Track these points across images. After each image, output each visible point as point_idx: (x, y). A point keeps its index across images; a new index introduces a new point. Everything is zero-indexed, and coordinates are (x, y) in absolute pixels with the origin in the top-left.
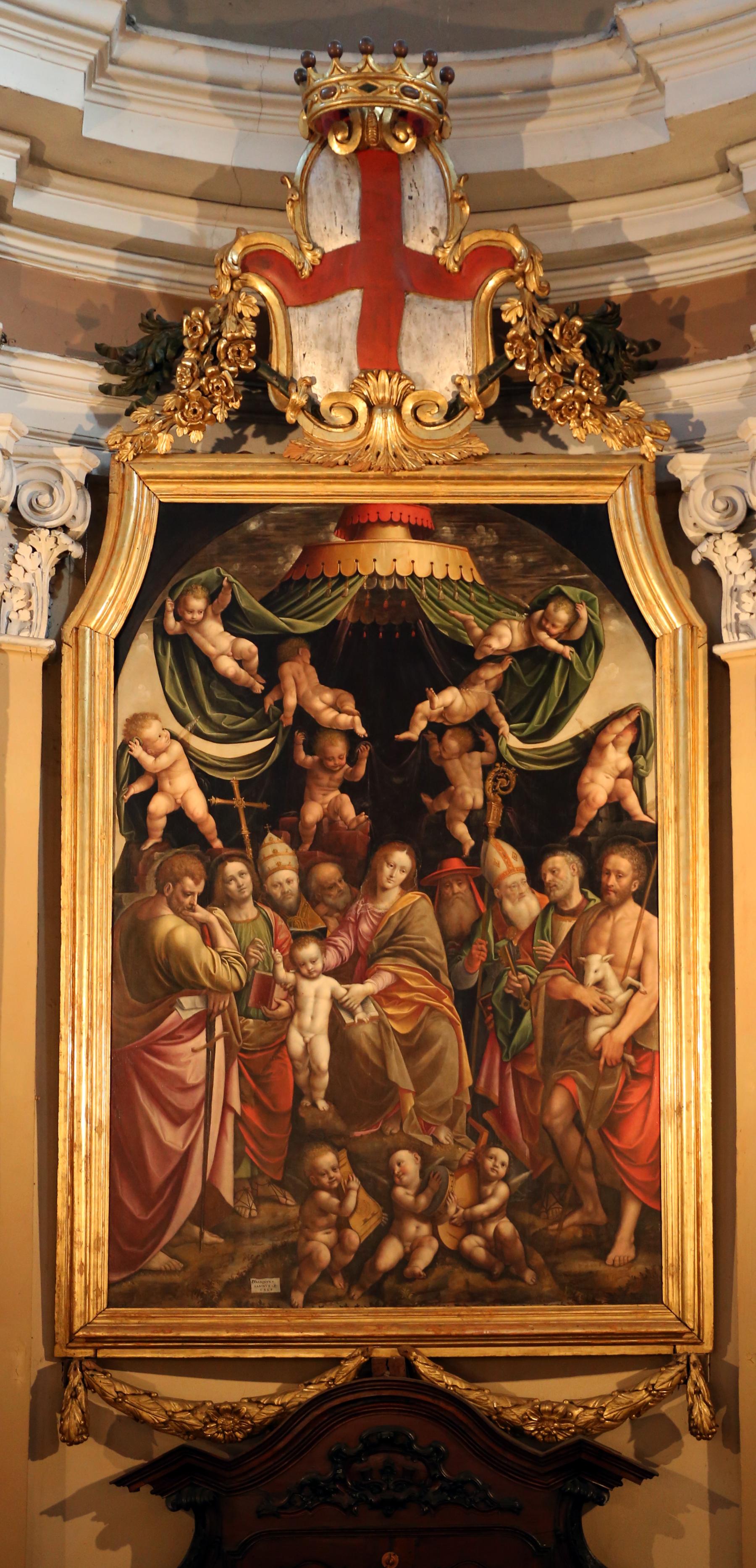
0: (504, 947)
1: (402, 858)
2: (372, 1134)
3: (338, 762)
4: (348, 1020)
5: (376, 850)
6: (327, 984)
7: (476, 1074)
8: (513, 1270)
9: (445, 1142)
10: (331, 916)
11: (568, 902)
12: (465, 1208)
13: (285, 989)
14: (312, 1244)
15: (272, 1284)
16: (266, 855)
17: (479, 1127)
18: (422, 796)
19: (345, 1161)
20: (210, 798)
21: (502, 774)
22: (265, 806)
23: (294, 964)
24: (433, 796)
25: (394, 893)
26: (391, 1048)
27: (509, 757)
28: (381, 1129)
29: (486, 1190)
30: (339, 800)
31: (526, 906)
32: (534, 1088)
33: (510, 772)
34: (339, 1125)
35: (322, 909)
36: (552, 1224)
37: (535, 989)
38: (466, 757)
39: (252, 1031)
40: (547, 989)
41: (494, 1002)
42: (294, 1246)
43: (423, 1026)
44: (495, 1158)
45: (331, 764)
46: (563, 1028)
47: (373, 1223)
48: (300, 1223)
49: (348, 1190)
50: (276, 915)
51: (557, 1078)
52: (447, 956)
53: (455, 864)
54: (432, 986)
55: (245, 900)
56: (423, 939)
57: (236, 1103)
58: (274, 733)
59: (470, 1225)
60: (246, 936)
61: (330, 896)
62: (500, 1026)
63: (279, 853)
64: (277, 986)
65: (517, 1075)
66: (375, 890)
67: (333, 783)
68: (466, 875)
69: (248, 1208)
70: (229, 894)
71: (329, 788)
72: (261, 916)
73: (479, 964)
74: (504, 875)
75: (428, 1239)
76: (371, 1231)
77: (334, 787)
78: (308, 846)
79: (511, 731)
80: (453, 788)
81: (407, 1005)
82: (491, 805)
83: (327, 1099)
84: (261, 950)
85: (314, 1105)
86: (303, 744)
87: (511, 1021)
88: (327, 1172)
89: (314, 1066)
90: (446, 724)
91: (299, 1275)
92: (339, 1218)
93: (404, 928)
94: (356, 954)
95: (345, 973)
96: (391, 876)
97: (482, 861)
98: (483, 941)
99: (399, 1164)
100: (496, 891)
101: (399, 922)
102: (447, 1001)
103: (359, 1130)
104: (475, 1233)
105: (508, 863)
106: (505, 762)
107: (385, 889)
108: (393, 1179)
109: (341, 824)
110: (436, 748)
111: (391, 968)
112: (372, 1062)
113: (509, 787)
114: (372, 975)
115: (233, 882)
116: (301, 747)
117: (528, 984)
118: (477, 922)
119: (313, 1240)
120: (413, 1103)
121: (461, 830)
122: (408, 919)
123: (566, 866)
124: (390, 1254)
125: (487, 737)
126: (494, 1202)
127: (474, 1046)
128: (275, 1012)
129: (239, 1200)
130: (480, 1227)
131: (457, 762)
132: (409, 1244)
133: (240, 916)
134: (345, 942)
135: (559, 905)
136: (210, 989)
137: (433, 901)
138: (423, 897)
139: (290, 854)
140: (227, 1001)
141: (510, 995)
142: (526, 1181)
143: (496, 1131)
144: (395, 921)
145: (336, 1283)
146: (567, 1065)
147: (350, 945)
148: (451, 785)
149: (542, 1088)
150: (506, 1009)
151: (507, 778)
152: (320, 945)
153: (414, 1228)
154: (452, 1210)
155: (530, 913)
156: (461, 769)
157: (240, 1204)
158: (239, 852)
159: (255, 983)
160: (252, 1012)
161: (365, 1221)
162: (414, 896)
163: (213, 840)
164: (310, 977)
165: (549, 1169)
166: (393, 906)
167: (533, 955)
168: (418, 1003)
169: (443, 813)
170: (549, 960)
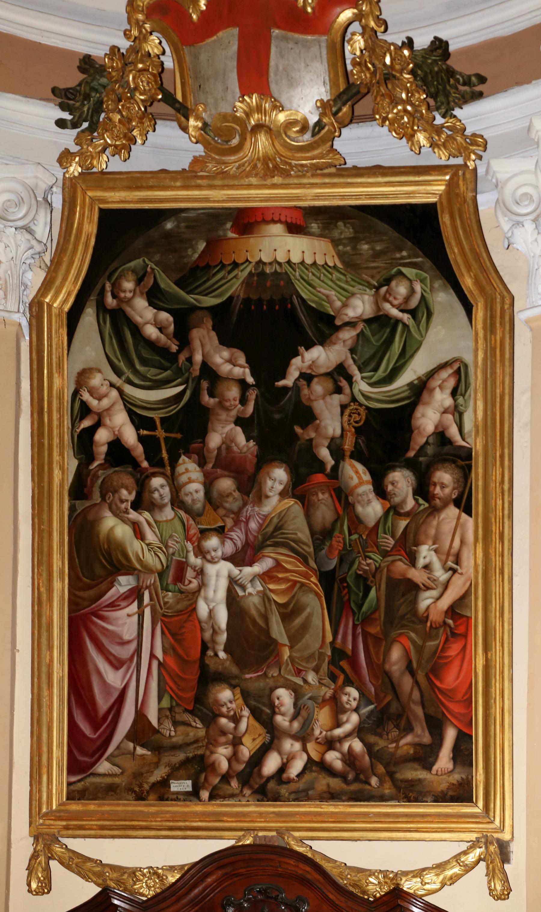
0: (356, 540)
2: (258, 676)
3: (233, 403)
4: (241, 593)
6: (226, 567)
7: (335, 634)
9: (312, 682)
10: (228, 517)
11: (404, 506)
12: (327, 731)
13: (195, 571)
15: (185, 785)
16: (180, 472)
17: (337, 672)
19: (239, 696)
20: (139, 430)
21: (355, 411)
22: (179, 436)
23: (200, 552)
24: (303, 427)
25: (274, 500)
26: (272, 613)
27: (360, 398)
28: (265, 673)
30: (233, 431)
31: (372, 509)
32: (378, 644)
33: (362, 410)
34: (234, 670)
35: (221, 512)
37: (379, 571)
38: (328, 398)
39: (171, 601)
40: (388, 570)
41: (348, 580)
42: (202, 757)
43: (296, 598)
44: (349, 694)
46: (400, 599)
47: (258, 743)
49: (241, 717)
50: (188, 516)
53: (320, 478)
54: (303, 568)
56: (296, 534)
57: (159, 653)
58: (186, 382)
61: (227, 502)
62: (353, 597)
63: (189, 470)
64: (189, 569)
65: (365, 634)
66: (261, 498)
69: (168, 729)
71: (227, 422)
72: (177, 517)
73: (337, 552)
74: (356, 487)
77: (230, 421)
78: (211, 465)
80: (318, 421)
82: (347, 435)
83: (225, 650)
84: (177, 542)
85: (216, 655)
87: (361, 594)
88: (226, 704)
89: (216, 627)
90: (313, 373)
91: (206, 779)
92: (234, 737)
94: (247, 544)
95: (239, 559)
96: (272, 488)
99: (278, 699)
100: (350, 499)
102: (314, 579)
103: (249, 673)
104: (334, 749)
105: (360, 478)
106: (358, 401)
107: (267, 497)
108: (274, 710)
109: (235, 449)
110: (305, 391)
111: (272, 555)
112: (259, 624)
113: (360, 420)
115: (156, 492)
116: (206, 392)
117: (374, 567)
118: (336, 521)
120: (288, 654)
121: (324, 453)
123: (403, 479)
126: (347, 727)
129: (162, 724)
130: (338, 745)
131: (321, 402)
134: (238, 536)
135: (397, 509)
136: (140, 571)
137: (303, 505)
138: (296, 502)
139: (198, 471)
140: (151, 579)
141: (360, 575)
142: (372, 712)
143: (350, 675)
144: (275, 520)
146: (403, 626)
147: (242, 538)
148: (316, 419)
149: (384, 643)
150: (358, 588)
151: (359, 414)
152: (219, 538)
153: (290, 745)
154: (317, 732)
155: (375, 514)
157: (162, 726)
158: (160, 470)
160: (171, 587)
161: (254, 740)
162: (290, 502)
163: (142, 462)
164: (212, 561)
165: (389, 704)
166: (274, 509)
169: (311, 440)
170: (389, 549)
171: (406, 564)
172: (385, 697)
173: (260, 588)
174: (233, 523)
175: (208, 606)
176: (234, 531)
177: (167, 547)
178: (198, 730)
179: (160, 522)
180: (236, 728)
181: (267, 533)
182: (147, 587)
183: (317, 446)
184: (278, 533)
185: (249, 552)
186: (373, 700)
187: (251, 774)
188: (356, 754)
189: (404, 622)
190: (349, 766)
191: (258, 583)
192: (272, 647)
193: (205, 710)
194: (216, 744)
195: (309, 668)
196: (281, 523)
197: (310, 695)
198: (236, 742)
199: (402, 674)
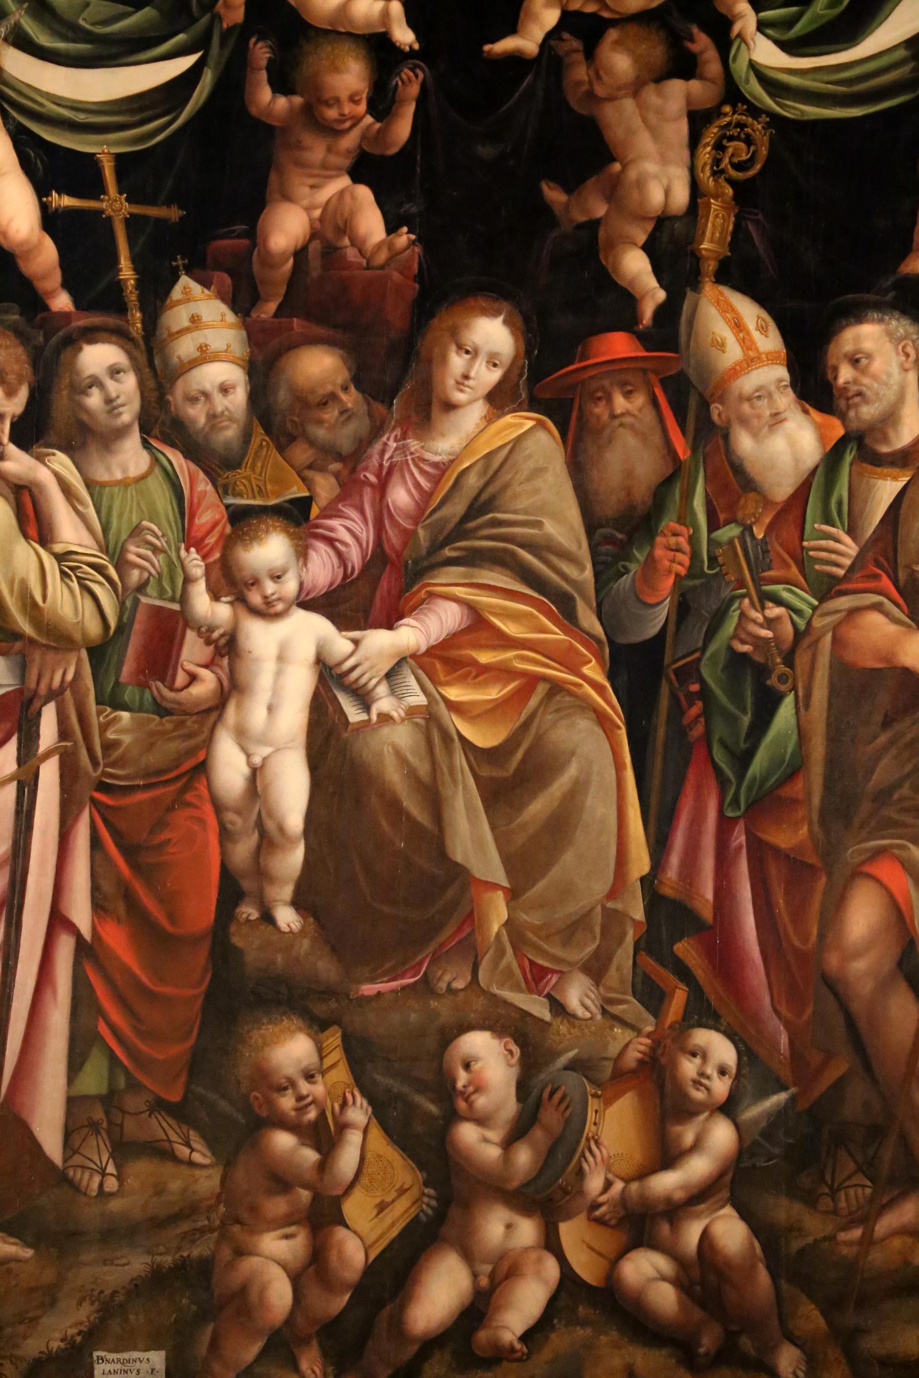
0: (731, 542)
1: (492, 334)
2: (404, 988)
3: (348, 109)
4: (354, 714)
5: (431, 315)
6: (309, 631)
7: (659, 845)
8: (746, 1344)
9: (580, 1012)
10: (322, 469)
11: (891, 434)
12: (627, 1181)
13: (208, 642)
14: (251, 1264)
15: (145, 1367)
16: (175, 329)
17: (666, 977)
18: (544, 187)
19: (336, 1055)
20: (48, 194)
21: (735, 132)
22: (173, 213)
23: (231, 582)
24: (571, 186)
25: (473, 415)
26: (455, 781)
27: (754, 89)
28: (425, 980)
29: (679, 1137)
30: (347, 198)
31: (786, 445)
32: (801, 884)
33: (757, 127)
34: (326, 968)
35: (302, 453)
36: (845, 1228)
37: (806, 642)
38: (651, 95)
39: (127, 739)
40: (835, 641)
41: (706, 672)
42: (204, 1270)
43: (533, 731)
44: (702, 1054)
45: (332, 113)
46: (875, 737)
47: (400, 1213)
48: (222, 1209)
49: (343, 1127)
50: (193, 466)
51: (857, 860)
52: (594, 565)
53: (618, 345)
54: (556, 635)
55: (121, 433)
56: (538, 524)
57: (81, 913)
58: (200, 44)
59: (640, 1224)
60: (121, 516)
61: (320, 422)
62: (720, 730)
63: (206, 328)
64: (190, 635)
65: (759, 852)
66: (428, 408)
67: (335, 160)
68: (644, 371)
69: (99, 1171)
70: (85, 417)
71: (327, 171)
72: (157, 471)
73: (670, 581)
74: (736, 372)
75: (533, 1255)
76: (394, 1233)
77: (339, 169)
78: (272, 307)
79: (762, 26)
80: (617, 167)
81: (497, 680)
82: (709, 205)
83: (297, 903)
84: (156, 550)
85: (268, 918)
86: (268, 69)
87: (746, 720)
88: (292, 1084)
89: (270, 825)
90: (606, 15)
91: (214, 1344)
92: (317, 1197)
93: (493, 498)
94: (378, 558)
95: (348, 605)
96: (466, 377)
97: (683, 338)
98: (683, 529)
99: (467, 1066)
100: (716, 409)
101: (482, 481)
102: (593, 670)
103: (372, 980)
104: (654, 1245)
105: (746, 342)
106: (745, 101)
107: (450, 407)
108: (451, 1103)
109: (351, 254)
110: (580, 72)
111: (460, 591)
112: (409, 816)
113: (752, 160)
114: (413, 609)
115: (95, 391)
116: (264, 75)
117: (789, 629)
118: (668, 482)
119: (251, 1254)
120: (504, 916)
121: (636, 265)
122: (505, 477)
123: (888, 347)
124: (441, 1292)
125: (702, 43)
126: (698, 1168)
127: (655, 782)
128: (183, 695)
129: (76, 1152)
130: (665, 1229)
131: (629, 104)
132: (488, 1268)
133: (109, 469)
134: (352, 531)
135: (867, 441)
136: (31, 641)
137: (563, 434)
138: (540, 423)
139: (231, 326)
140: (72, 668)
141: (744, 655)
142: (778, 1117)
143: (707, 989)
144: (473, 481)
145: (304, 1366)
146: (886, 826)
147: (363, 536)
148: (612, 159)
149: (822, 883)
150: (736, 696)
151: (749, 141)
152: (291, 536)
153: (502, 1228)
154: (594, 1184)
155: (797, 461)
156: (637, 122)
157: (77, 1159)
158: (111, 320)
159: (137, 627)
160: (129, 694)
161: (382, 1207)
162: (520, 422)
163: (52, 294)
164: (267, 612)
165: (839, 1085)
166: (469, 446)
167: (801, 560)
168: (524, 674)
169: (593, 225)
170: (841, 572)
171: (897, 621)
172: (825, 1063)
173: (420, 700)
174: (337, 491)
175: (248, 756)
176: (339, 515)
177: (121, 564)
178: (198, 1172)
179: (103, 485)
180: (323, 1166)
181: (445, 520)
182: (54, 695)
183: (611, 245)
184: (480, 521)
185: (384, 584)
186: (785, 1073)
187: (366, 1332)
188: (728, 1263)
189: (887, 812)
190: (703, 1306)
191: (412, 681)
192: (450, 893)
193: (223, 1105)
194: (258, 1222)
195: (570, 964)
196: (491, 490)
197: (571, 1054)
198: (323, 1216)
199: (883, 987)
